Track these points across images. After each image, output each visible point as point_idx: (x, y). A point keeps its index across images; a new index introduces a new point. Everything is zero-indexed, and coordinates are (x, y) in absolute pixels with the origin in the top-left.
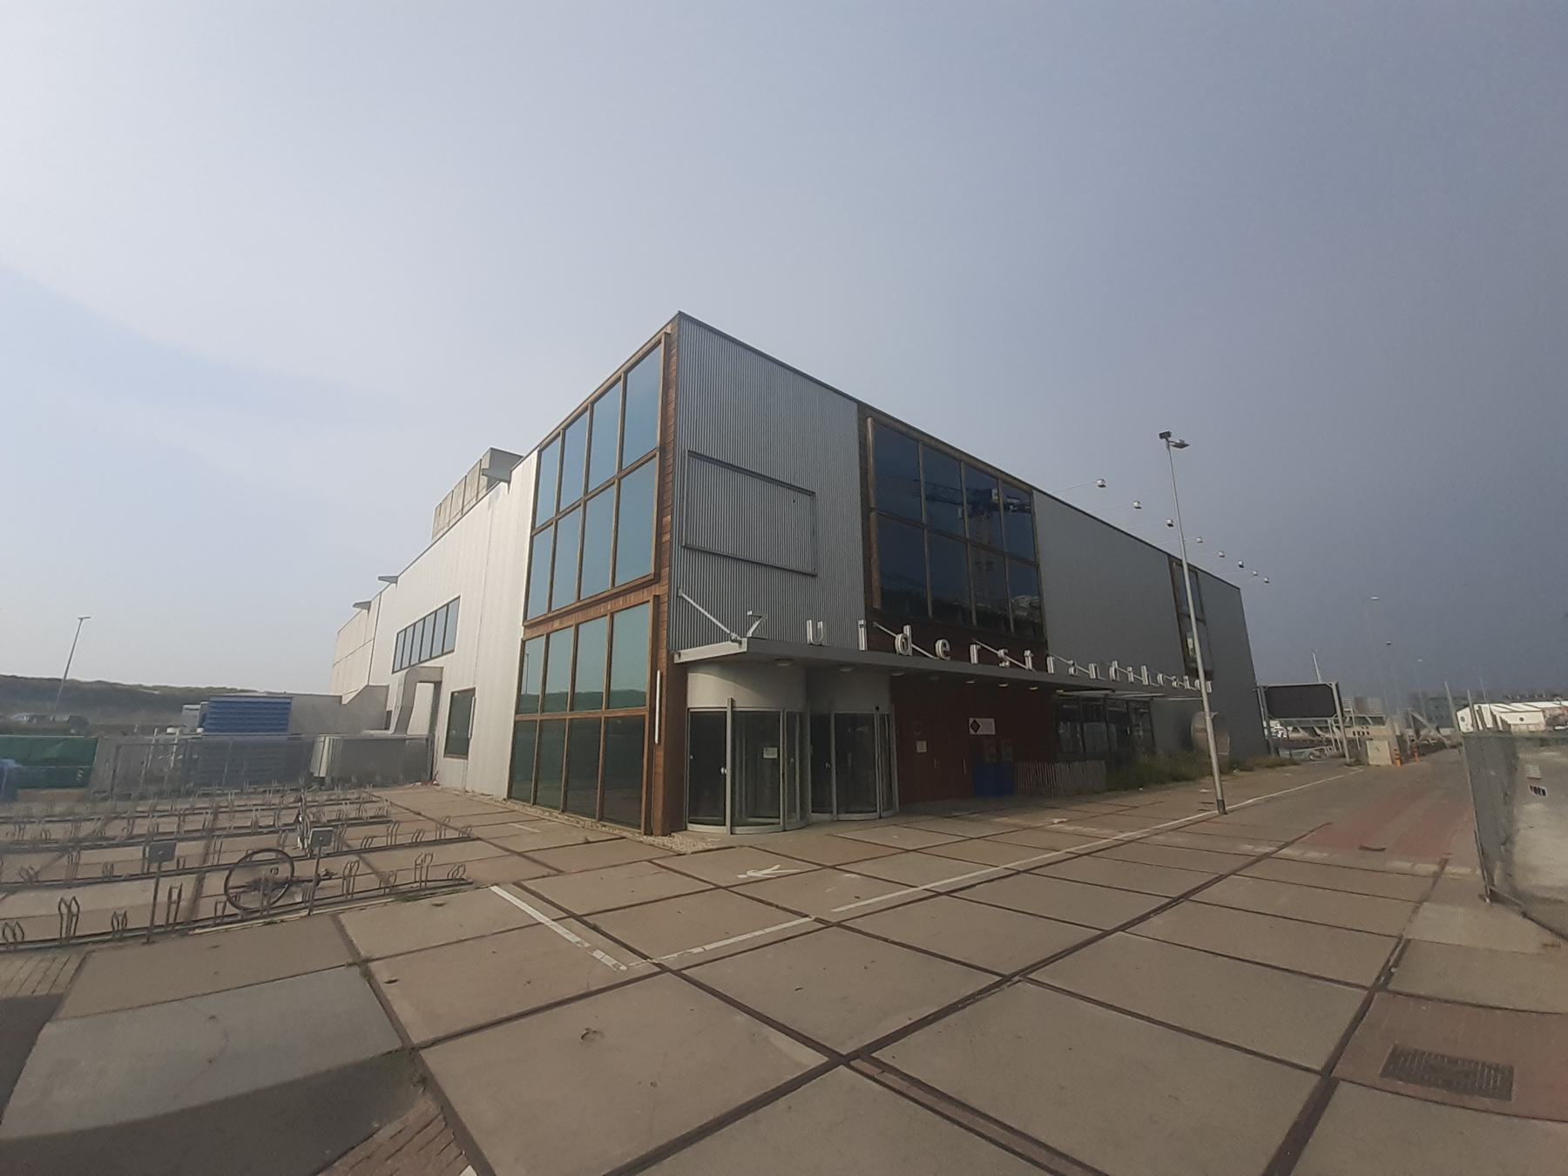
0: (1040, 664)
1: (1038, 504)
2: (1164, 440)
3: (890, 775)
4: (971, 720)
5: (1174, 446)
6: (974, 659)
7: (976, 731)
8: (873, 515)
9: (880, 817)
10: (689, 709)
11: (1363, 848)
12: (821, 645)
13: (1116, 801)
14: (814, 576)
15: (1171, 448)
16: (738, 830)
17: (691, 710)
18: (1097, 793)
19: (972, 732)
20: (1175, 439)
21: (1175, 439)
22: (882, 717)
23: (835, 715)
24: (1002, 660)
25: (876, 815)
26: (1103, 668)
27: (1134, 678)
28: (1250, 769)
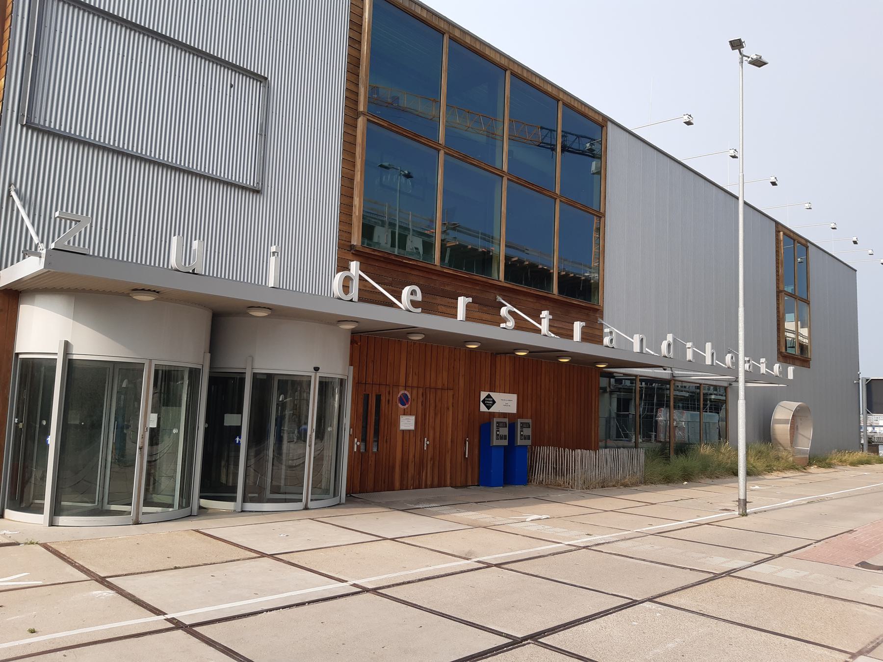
0: (593, 335)
1: (613, 139)
2: (737, 51)
3: (24, 460)
4: (483, 395)
5: (750, 63)
6: (577, 335)
7: (489, 408)
8: (361, 122)
9: (306, 508)
10: (17, 354)
11: (864, 565)
12: (613, 348)
13: (348, 521)
14: (257, 192)
15: (745, 63)
16: (62, 520)
17: (21, 356)
18: (626, 486)
19: (483, 408)
20: (750, 51)
21: (750, 51)
22: (325, 386)
23: (279, 380)
24: (504, 321)
25: (300, 505)
26: (784, 372)
27: (766, 371)
28: (829, 466)
